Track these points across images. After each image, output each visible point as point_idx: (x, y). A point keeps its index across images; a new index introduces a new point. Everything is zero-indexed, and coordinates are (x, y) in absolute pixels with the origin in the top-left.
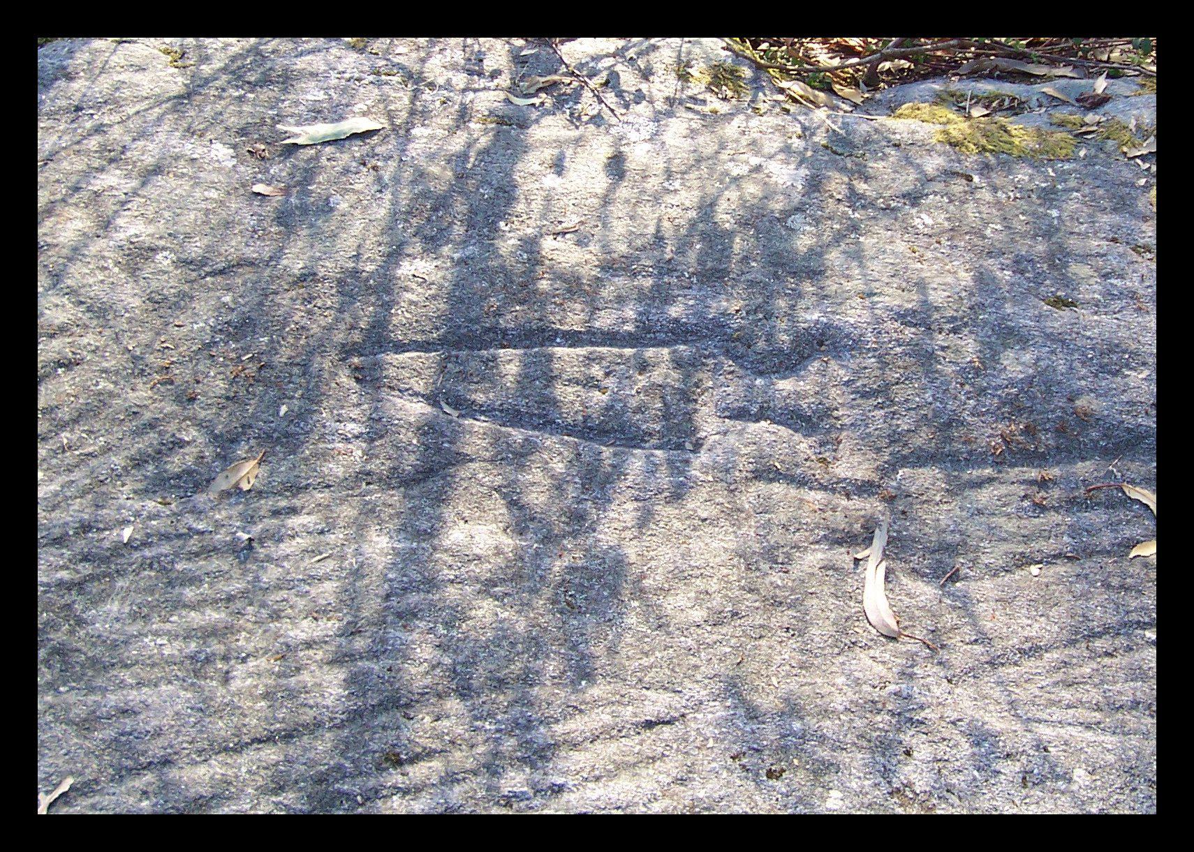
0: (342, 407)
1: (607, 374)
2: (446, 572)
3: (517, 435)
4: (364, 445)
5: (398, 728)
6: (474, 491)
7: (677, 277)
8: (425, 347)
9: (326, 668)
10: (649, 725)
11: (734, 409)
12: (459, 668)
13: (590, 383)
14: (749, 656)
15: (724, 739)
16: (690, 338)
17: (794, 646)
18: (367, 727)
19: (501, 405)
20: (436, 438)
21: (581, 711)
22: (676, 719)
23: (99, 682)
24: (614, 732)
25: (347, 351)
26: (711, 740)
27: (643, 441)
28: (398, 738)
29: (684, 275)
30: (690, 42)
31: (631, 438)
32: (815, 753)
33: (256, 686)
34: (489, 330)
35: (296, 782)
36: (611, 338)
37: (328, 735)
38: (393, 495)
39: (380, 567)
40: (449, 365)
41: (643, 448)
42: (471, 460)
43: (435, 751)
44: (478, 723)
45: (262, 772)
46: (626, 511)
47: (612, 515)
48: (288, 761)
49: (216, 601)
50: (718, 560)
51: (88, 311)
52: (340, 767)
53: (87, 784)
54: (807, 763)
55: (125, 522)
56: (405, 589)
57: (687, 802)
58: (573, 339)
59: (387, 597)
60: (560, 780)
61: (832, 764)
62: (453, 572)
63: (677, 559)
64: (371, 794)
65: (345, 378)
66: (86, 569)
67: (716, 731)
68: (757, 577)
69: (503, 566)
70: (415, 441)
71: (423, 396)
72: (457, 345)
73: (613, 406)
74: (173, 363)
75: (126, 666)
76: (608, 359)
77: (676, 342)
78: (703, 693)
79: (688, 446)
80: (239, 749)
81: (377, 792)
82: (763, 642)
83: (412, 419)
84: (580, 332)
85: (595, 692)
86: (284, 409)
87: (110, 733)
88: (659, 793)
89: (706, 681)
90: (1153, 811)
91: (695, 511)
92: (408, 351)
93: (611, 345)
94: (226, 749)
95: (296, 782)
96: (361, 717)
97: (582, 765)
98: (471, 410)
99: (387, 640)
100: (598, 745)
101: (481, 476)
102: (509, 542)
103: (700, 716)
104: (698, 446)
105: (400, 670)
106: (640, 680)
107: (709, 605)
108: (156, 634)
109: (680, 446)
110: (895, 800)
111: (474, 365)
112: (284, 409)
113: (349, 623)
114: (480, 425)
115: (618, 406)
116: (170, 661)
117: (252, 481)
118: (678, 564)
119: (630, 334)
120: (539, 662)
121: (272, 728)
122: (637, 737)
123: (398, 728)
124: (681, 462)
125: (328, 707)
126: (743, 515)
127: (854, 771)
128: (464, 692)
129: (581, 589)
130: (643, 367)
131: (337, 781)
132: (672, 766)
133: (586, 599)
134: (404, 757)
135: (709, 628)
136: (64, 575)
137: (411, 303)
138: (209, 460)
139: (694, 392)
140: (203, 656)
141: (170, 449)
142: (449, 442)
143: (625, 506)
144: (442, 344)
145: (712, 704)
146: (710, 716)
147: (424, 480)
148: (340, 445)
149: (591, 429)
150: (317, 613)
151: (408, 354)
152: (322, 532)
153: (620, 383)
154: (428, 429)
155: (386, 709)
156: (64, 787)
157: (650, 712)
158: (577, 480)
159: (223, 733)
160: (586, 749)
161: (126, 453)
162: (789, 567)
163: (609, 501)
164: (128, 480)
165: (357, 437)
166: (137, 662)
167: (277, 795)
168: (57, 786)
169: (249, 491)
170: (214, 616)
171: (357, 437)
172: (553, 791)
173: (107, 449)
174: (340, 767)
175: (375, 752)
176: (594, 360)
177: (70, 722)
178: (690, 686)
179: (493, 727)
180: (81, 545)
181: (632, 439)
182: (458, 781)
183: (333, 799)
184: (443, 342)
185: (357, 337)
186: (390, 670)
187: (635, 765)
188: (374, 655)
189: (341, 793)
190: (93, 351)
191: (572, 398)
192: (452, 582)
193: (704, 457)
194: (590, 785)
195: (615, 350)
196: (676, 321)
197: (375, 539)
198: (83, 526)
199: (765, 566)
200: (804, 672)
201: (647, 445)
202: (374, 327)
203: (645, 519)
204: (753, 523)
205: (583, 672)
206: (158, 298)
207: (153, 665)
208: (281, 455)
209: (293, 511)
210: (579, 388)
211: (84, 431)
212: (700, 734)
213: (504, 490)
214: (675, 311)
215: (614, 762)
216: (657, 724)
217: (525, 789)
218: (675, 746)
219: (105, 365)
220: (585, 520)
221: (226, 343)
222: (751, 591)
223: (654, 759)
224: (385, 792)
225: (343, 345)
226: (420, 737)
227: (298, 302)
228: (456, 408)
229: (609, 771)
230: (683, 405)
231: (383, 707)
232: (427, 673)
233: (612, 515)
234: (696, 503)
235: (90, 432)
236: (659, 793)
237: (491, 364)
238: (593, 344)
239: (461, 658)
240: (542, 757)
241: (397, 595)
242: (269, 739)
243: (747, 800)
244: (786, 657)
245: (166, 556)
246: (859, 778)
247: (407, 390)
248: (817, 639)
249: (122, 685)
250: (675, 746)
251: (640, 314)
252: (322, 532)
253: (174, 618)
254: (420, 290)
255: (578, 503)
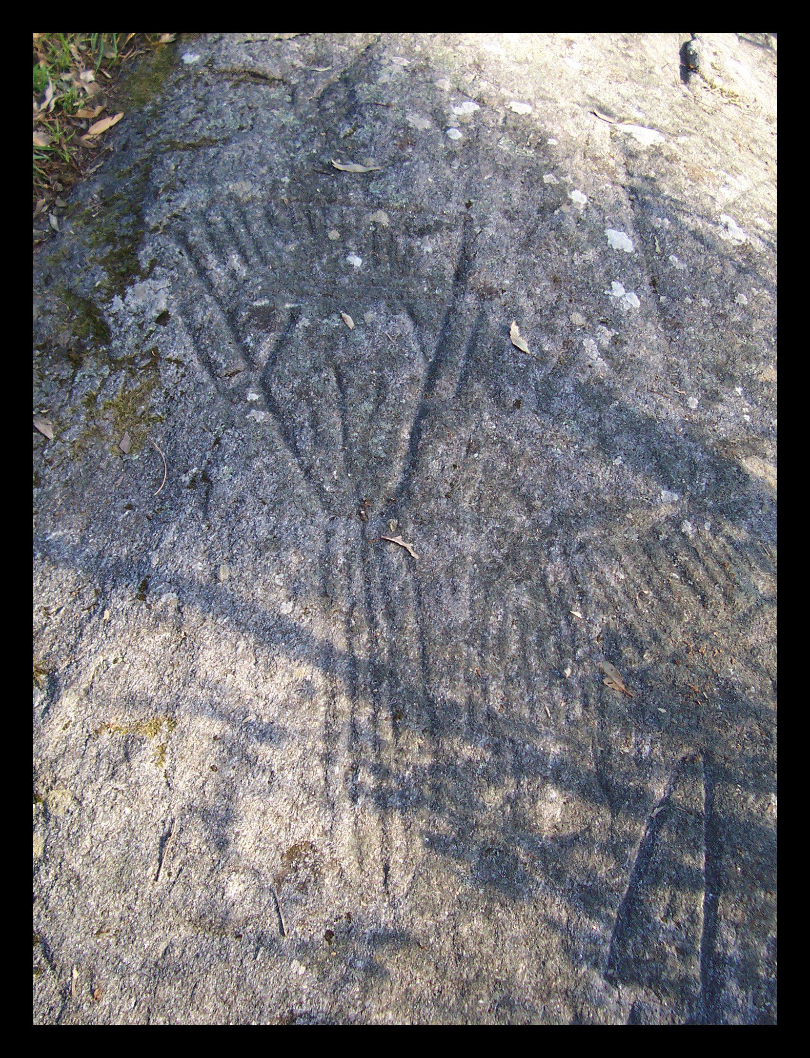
0: (662, 745)
1: (678, 924)
2: (526, 780)
3: (633, 853)
4: (633, 755)
5: (418, 723)
6: (589, 813)
7: (766, 996)
8: (709, 803)
9: (467, 696)
10: (386, 869)
11: (639, 1015)
12: (452, 767)
13: (671, 911)
14: (424, 954)
15: (364, 913)
16: (707, 995)
17: (426, 992)
18: (421, 707)
19: (657, 845)
20: (633, 797)
21: (406, 830)
22: (386, 887)
23: (477, 582)
24: (386, 845)
25: (708, 755)
26: (365, 905)
27: (619, 939)
28: (411, 721)
29: (767, 1001)
30: (280, 40)
31: (621, 932)
32: (337, 969)
33: (461, 656)
34: (721, 848)
35: (394, 662)
36: (711, 932)
37: (421, 685)
38: (591, 764)
39: (535, 741)
40: (693, 817)
41: (612, 938)
42: (613, 816)
43: (398, 739)
44: (411, 768)
45: (403, 647)
46: (560, 910)
47: (558, 900)
48: (408, 661)
49: (524, 651)
50: (507, 961)
51: (745, 615)
52: (398, 684)
53: (414, 565)
54: (331, 961)
55: (585, 614)
56: (516, 752)
57: (324, 870)
58: (711, 906)
59: (512, 741)
60: (360, 801)
61: (325, 977)
62: (525, 785)
63: (513, 933)
64: (377, 697)
65: (687, 750)
66: (554, 590)
67: (371, 910)
68: (488, 986)
69: (526, 816)
70: (631, 784)
71: (669, 796)
72: (709, 825)
73: (650, 922)
74: (703, 654)
75: (486, 597)
76: (691, 927)
77: (705, 983)
78: (402, 912)
79: (611, 971)
80: (421, 639)
81: (378, 700)
82: (432, 968)
83: (649, 785)
84: (716, 910)
85: (418, 842)
86: (663, 711)
87: (443, 581)
88: (335, 856)
89: (410, 917)
90: (36, 1022)
91: (552, 959)
92: (706, 792)
93: (705, 933)
94: (422, 633)
95: (394, 662)
96: (430, 705)
97: (367, 817)
98: (656, 825)
99: (481, 733)
100: (379, 833)
101: (600, 820)
102: (547, 831)
103: (385, 904)
104: (609, 979)
105: (457, 733)
106: (421, 874)
107: (470, 941)
108: (505, 616)
109: (611, 965)
110: (286, 1014)
111: (692, 835)
112: (663, 711)
113: (496, 715)
114: (642, 831)
115: (650, 926)
116: (486, 619)
117: (610, 686)
118: (509, 932)
119: (713, 948)
120: (447, 816)
121: (430, 657)
122: (380, 859)
123: (418, 723)
124: (596, 960)
125: (438, 687)
126: (545, 996)
127: (315, 992)
128: (435, 769)
129: (499, 862)
130: (684, 953)
131: (390, 682)
132: (352, 872)
133: (492, 861)
134: (398, 721)
135: (452, 934)
136: (551, 579)
137: (746, 799)
138: (629, 666)
139: (657, 986)
140: (486, 634)
141: (638, 647)
142: (629, 805)
143: (564, 911)
144: (710, 815)
145: (392, 915)
146: (384, 911)
147: (601, 786)
148: (633, 740)
149: (633, 904)
150: (507, 704)
151: (703, 792)
152: (567, 717)
153: (670, 931)
154: (641, 796)
155: (432, 720)
156: (413, 554)
157: (396, 874)
158: (590, 883)
159: (432, 632)
160: (378, 824)
161: (635, 622)
162: (493, 1014)
163: (569, 901)
164: (617, 621)
165: (639, 751)
166: (487, 603)
167: (388, 651)
168: (416, 552)
169: (603, 684)
170: (513, 648)
171: (639, 751)
172: (354, 796)
173: (639, 613)
174: (398, 684)
175: (404, 705)
176: (692, 917)
177: (452, 564)
178: (409, 904)
179: (407, 775)
180: (570, 589)
181: (621, 931)
182: (375, 746)
183: (378, 677)
184: (713, 816)
185: (719, 760)
186: (459, 728)
187: (360, 850)
188: (470, 723)
189: (381, 683)
190: (713, 615)
191: (660, 893)
192: (519, 782)
193: (599, 982)
194: (353, 819)
195: (700, 935)
196: (723, 985)
197: (558, 746)
198: (583, 592)
199: (497, 996)
200: (403, 990)
201: (615, 941)
202: (726, 772)
203: (553, 924)
204: (537, 1001)
205: (434, 843)
206: (755, 652)
207: (484, 610)
208: (629, 705)
209: (586, 706)
210: (668, 901)
211: (653, 603)
212: (372, 899)
213: (587, 833)
214: (732, 985)
215: (365, 837)
216: (386, 874)
217: (359, 779)
218: (367, 880)
219: (702, 619)
220: (556, 880)
221: (718, 686)
222: (477, 976)
223: (361, 863)
224: (377, 705)
225: (712, 752)
226: (409, 733)
227: (749, 730)
228: (657, 816)
229: (359, 833)
230: (646, 975)
231: (433, 718)
232: (452, 748)
233: (558, 900)
234: (556, 963)
235: (652, 606)
236: (335, 856)
237: (692, 844)
238: (706, 920)
239: (459, 770)
240: (379, 797)
241: (513, 747)
242: (424, 656)
243: (314, 910)
244: (418, 982)
245: (560, 632)
246: (309, 993)
247: (675, 788)
248: (427, 1010)
249: (473, 593)
250: (367, 880)
251: (731, 958)
252: (567, 717)
253: (515, 627)
254: (757, 806)
255: (571, 880)
